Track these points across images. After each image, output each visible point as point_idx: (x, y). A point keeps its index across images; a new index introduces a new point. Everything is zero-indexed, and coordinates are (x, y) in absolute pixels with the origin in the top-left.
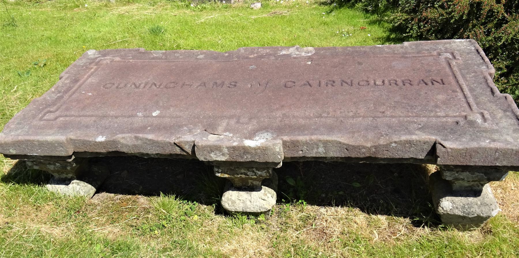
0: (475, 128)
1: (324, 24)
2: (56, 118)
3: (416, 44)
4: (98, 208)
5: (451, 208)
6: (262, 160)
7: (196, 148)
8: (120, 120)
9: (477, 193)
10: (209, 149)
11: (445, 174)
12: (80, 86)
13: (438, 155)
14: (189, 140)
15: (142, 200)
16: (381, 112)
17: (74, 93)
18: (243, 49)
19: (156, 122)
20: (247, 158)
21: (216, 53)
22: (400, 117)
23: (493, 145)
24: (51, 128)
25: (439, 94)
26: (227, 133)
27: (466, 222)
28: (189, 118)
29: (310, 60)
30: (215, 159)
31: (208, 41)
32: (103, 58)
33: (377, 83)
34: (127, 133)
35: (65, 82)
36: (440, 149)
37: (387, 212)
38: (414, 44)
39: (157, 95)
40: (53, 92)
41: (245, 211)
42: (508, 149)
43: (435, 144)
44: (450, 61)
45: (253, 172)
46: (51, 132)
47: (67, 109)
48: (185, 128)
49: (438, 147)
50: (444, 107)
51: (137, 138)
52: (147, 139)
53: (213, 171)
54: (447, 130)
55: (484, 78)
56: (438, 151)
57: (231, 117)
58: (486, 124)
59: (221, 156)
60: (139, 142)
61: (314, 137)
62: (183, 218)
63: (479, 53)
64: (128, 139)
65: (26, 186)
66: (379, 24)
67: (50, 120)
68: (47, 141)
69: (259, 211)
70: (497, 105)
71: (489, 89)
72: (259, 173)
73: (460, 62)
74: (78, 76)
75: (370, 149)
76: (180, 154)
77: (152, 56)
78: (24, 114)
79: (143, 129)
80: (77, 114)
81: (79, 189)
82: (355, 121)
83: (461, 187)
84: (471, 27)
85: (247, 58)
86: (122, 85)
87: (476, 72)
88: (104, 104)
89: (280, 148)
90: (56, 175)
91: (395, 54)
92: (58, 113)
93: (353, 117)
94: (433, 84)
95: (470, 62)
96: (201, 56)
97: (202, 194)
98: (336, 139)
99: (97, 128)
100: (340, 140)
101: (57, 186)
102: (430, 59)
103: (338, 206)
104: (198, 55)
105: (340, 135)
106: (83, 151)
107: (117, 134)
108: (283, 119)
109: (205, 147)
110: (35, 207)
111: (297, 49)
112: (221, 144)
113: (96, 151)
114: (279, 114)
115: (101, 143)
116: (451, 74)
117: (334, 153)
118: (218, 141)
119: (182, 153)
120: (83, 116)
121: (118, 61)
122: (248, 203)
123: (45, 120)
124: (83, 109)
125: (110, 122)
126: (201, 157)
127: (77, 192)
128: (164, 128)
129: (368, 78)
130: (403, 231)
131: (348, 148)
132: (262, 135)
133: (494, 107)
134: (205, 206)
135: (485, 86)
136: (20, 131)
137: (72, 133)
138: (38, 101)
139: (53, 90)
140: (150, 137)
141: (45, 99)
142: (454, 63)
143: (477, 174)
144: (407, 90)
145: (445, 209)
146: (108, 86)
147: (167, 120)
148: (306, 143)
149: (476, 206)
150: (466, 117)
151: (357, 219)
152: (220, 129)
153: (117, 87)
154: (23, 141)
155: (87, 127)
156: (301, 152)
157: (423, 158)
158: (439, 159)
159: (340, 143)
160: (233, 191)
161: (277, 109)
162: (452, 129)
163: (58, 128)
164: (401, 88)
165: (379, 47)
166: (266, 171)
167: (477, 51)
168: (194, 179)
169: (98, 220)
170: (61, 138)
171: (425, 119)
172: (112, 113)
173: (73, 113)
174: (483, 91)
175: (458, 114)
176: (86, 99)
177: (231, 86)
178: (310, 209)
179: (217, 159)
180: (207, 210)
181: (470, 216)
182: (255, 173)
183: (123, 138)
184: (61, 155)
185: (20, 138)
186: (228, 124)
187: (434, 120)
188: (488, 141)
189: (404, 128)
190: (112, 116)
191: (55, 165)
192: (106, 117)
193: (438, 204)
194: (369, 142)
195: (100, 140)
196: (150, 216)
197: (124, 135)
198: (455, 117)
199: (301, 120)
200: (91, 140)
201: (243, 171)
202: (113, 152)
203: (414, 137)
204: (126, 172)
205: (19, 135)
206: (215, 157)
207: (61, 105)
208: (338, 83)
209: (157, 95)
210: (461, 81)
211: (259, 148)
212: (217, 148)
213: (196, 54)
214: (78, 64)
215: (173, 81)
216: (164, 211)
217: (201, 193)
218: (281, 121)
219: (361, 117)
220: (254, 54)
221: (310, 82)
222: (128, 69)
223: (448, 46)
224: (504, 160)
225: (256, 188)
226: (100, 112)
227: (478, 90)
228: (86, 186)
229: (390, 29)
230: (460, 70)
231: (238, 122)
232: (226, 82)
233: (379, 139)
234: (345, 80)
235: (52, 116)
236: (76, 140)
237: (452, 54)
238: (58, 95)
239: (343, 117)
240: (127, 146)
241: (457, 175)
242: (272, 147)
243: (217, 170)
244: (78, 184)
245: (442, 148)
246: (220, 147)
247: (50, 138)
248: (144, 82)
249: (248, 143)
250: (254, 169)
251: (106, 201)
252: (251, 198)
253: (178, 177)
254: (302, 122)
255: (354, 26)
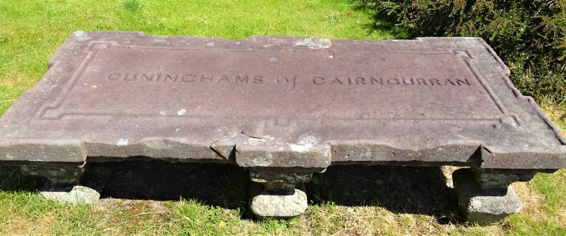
0: (512, 131)
1: (310, 7)
2: (60, 117)
3: (429, 40)
4: (106, 216)
5: (480, 206)
6: (308, 166)
7: (237, 153)
8: (140, 120)
9: (503, 192)
10: (252, 155)
11: (482, 176)
12: (79, 77)
13: (483, 159)
14: (228, 144)
15: (156, 205)
16: (420, 114)
17: (73, 84)
18: (255, 37)
19: (183, 122)
20: (293, 164)
21: (226, 41)
22: (440, 119)
23: (534, 150)
24: (57, 128)
25: (468, 95)
26: (268, 137)
27: (485, 219)
28: (221, 117)
29: (331, 53)
30: (257, 165)
31: (193, 21)
32: (96, 42)
33: (406, 81)
34: (153, 136)
35: (58, 70)
36: (486, 154)
37: (413, 210)
38: (427, 40)
39: (176, 90)
40: (46, 83)
41: (277, 215)
42: (546, 154)
43: (479, 149)
44: (467, 60)
45: (293, 176)
46: (59, 133)
47: (72, 105)
48: (219, 130)
49: (484, 152)
50: (478, 109)
51: (166, 142)
52: (179, 143)
53: (249, 176)
54: (486, 133)
55: (503, 78)
56: (483, 156)
57: (267, 118)
58: (520, 127)
59: (265, 162)
60: (170, 147)
61: (363, 142)
62: (208, 225)
63: (490, 52)
64: (156, 143)
65: (15, 192)
66: (364, 10)
67: (53, 119)
68: (57, 146)
69: (292, 215)
70: (522, 107)
71: (510, 91)
72: (300, 177)
73: (476, 61)
74: (71, 63)
75: (416, 153)
76: (216, 159)
77: (154, 42)
78: (16, 111)
79: (170, 131)
80: (85, 111)
81: (84, 195)
82: (396, 124)
83: (489, 186)
84: (461, 21)
85: (262, 48)
86: (130, 77)
87: (492, 72)
88: (116, 99)
89: (328, 154)
90: (54, 181)
91: (412, 49)
92: (61, 110)
93: (394, 119)
94: (459, 84)
95: (484, 61)
96: (211, 44)
97: (222, 196)
98: (384, 143)
99: (114, 129)
100: (389, 145)
101: (56, 193)
102: (448, 57)
103: (365, 206)
104: (207, 42)
105: (387, 139)
106: (99, 155)
107: (142, 137)
108: (323, 120)
109: (248, 152)
110: (31, 219)
111: (313, 40)
112: (266, 150)
113: (115, 156)
114: (318, 114)
115: (123, 147)
116: (472, 73)
117: (381, 157)
118: (261, 145)
119: (218, 158)
120: (93, 114)
121: (117, 47)
122: (281, 207)
123: (45, 119)
124: (92, 105)
125: (129, 122)
126: (241, 162)
127: (81, 199)
128: (195, 129)
129: (396, 76)
130: (431, 228)
131: (395, 152)
132: (306, 138)
133: (521, 110)
134: (229, 210)
135: (507, 88)
136: (17, 132)
137: (86, 136)
138: (30, 94)
139: (46, 80)
140: (183, 140)
141: (38, 91)
142: (471, 62)
143: (511, 175)
144: (437, 90)
145: (475, 208)
146: (114, 77)
147: (196, 121)
148: (355, 148)
149: (503, 204)
150: (500, 120)
151: (386, 218)
152: (259, 131)
153: (125, 79)
154: (25, 146)
155: (102, 127)
156: (347, 156)
157: (465, 161)
158: (483, 163)
159: (389, 147)
160: (264, 195)
161: (315, 109)
162: (490, 133)
163: (66, 128)
164: (431, 88)
165: (395, 42)
166: (307, 175)
167: (488, 50)
168: (224, 182)
169: (110, 231)
170: (76, 142)
171: (464, 122)
172: (129, 111)
173: (80, 110)
174: (506, 92)
175: (492, 117)
176: (91, 92)
177: (256, 81)
178: (339, 210)
179: (259, 165)
180: (233, 215)
181: (496, 214)
182: (295, 178)
183: (150, 142)
184: (72, 161)
185: (21, 142)
186: (266, 126)
187: (472, 123)
188: (527, 146)
189: (445, 131)
190: (130, 115)
191: (59, 170)
192: (123, 115)
193: (468, 203)
194: (416, 147)
195: (121, 143)
196: (171, 224)
197: (151, 139)
198: (490, 120)
199: (342, 121)
200: (110, 143)
201: (282, 176)
202: (135, 156)
203: (460, 142)
204: (130, 172)
205: (17, 138)
206: (257, 163)
207: (62, 101)
208: (368, 80)
209: (176, 90)
210: (484, 82)
211: (307, 153)
212: (262, 154)
213: (204, 41)
214: (67, 48)
215: (189, 73)
216: (188, 218)
217: (221, 195)
218: (322, 123)
219: (401, 119)
220: (268, 43)
221: (339, 79)
222: (132, 55)
223: (458, 43)
224: (541, 164)
225: (289, 191)
226: (113, 109)
227: (501, 92)
228: (91, 192)
229: (376, 16)
230: (478, 69)
231: (276, 123)
232: (250, 77)
233: (425, 143)
234: (374, 77)
235: (54, 114)
236: (92, 144)
237: (467, 52)
238: (53, 86)
239: (384, 119)
240: (154, 150)
241: (493, 176)
242: (321, 153)
243: (253, 175)
244: (82, 190)
245: (488, 153)
246: (265, 152)
247: (60, 142)
248: (155, 73)
249: (295, 148)
250: (295, 174)
251: (113, 207)
252: (285, 202)
253: (191, 177)
254: (345, 124)
255: (340, 11)
